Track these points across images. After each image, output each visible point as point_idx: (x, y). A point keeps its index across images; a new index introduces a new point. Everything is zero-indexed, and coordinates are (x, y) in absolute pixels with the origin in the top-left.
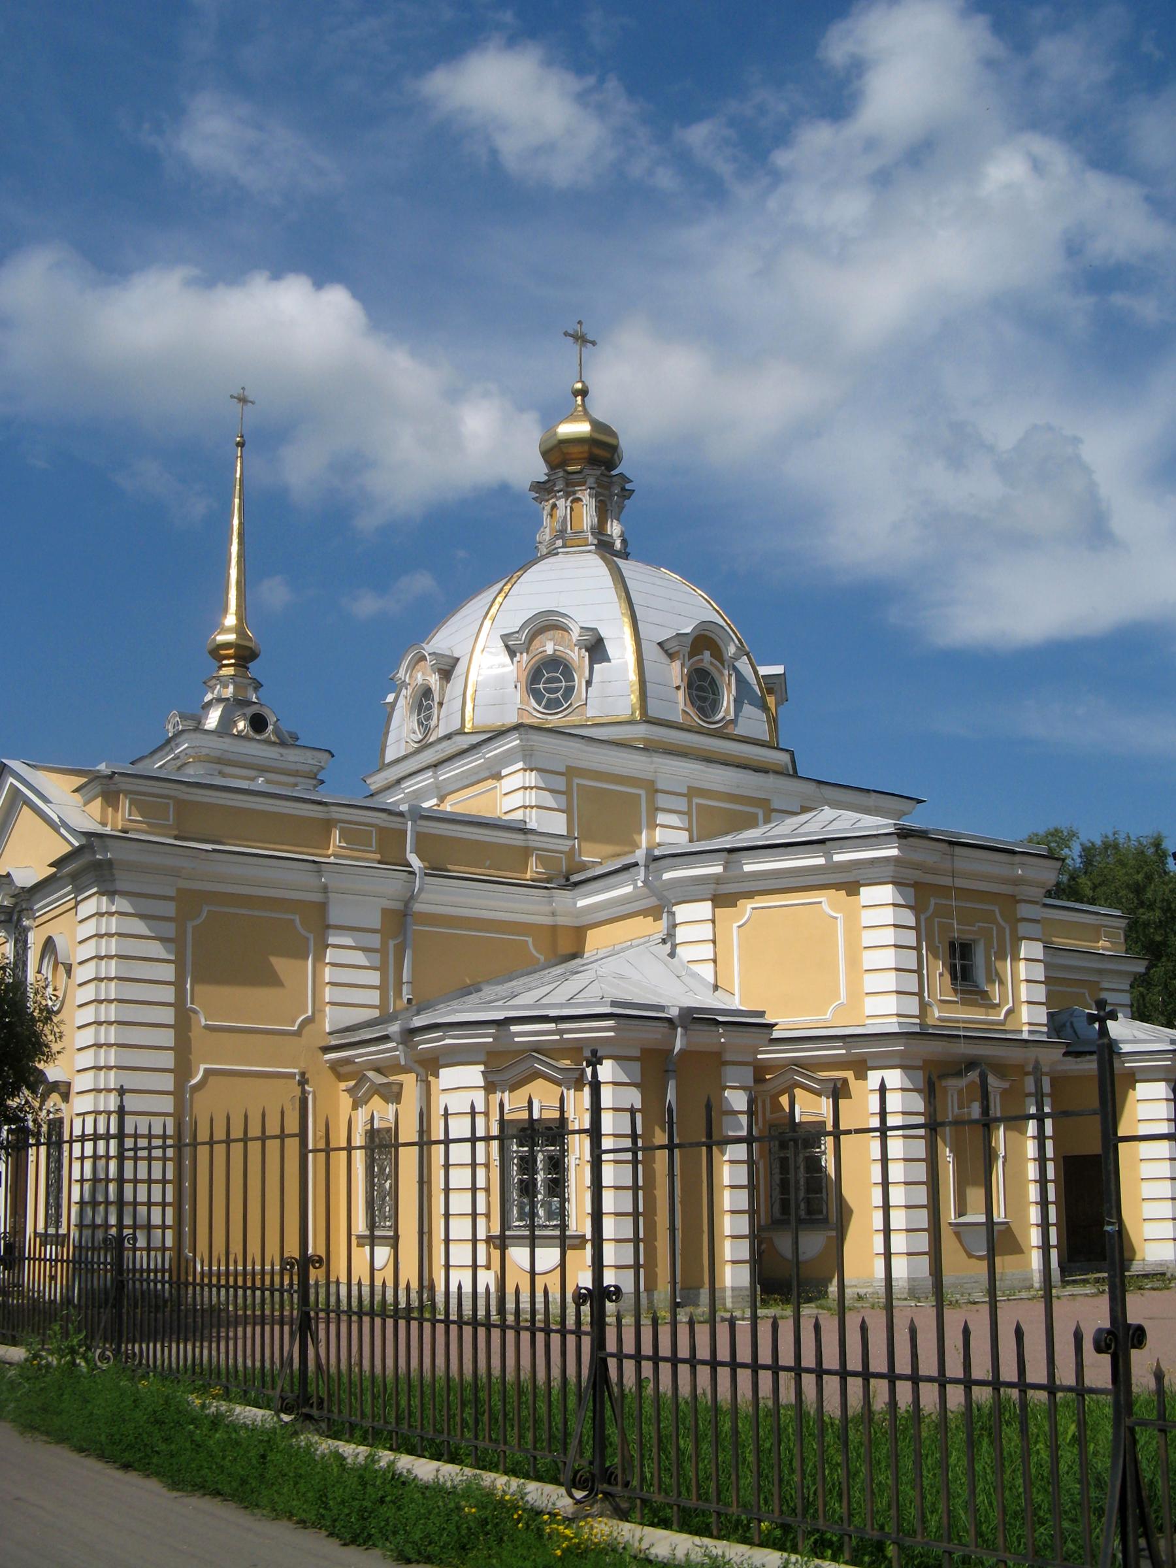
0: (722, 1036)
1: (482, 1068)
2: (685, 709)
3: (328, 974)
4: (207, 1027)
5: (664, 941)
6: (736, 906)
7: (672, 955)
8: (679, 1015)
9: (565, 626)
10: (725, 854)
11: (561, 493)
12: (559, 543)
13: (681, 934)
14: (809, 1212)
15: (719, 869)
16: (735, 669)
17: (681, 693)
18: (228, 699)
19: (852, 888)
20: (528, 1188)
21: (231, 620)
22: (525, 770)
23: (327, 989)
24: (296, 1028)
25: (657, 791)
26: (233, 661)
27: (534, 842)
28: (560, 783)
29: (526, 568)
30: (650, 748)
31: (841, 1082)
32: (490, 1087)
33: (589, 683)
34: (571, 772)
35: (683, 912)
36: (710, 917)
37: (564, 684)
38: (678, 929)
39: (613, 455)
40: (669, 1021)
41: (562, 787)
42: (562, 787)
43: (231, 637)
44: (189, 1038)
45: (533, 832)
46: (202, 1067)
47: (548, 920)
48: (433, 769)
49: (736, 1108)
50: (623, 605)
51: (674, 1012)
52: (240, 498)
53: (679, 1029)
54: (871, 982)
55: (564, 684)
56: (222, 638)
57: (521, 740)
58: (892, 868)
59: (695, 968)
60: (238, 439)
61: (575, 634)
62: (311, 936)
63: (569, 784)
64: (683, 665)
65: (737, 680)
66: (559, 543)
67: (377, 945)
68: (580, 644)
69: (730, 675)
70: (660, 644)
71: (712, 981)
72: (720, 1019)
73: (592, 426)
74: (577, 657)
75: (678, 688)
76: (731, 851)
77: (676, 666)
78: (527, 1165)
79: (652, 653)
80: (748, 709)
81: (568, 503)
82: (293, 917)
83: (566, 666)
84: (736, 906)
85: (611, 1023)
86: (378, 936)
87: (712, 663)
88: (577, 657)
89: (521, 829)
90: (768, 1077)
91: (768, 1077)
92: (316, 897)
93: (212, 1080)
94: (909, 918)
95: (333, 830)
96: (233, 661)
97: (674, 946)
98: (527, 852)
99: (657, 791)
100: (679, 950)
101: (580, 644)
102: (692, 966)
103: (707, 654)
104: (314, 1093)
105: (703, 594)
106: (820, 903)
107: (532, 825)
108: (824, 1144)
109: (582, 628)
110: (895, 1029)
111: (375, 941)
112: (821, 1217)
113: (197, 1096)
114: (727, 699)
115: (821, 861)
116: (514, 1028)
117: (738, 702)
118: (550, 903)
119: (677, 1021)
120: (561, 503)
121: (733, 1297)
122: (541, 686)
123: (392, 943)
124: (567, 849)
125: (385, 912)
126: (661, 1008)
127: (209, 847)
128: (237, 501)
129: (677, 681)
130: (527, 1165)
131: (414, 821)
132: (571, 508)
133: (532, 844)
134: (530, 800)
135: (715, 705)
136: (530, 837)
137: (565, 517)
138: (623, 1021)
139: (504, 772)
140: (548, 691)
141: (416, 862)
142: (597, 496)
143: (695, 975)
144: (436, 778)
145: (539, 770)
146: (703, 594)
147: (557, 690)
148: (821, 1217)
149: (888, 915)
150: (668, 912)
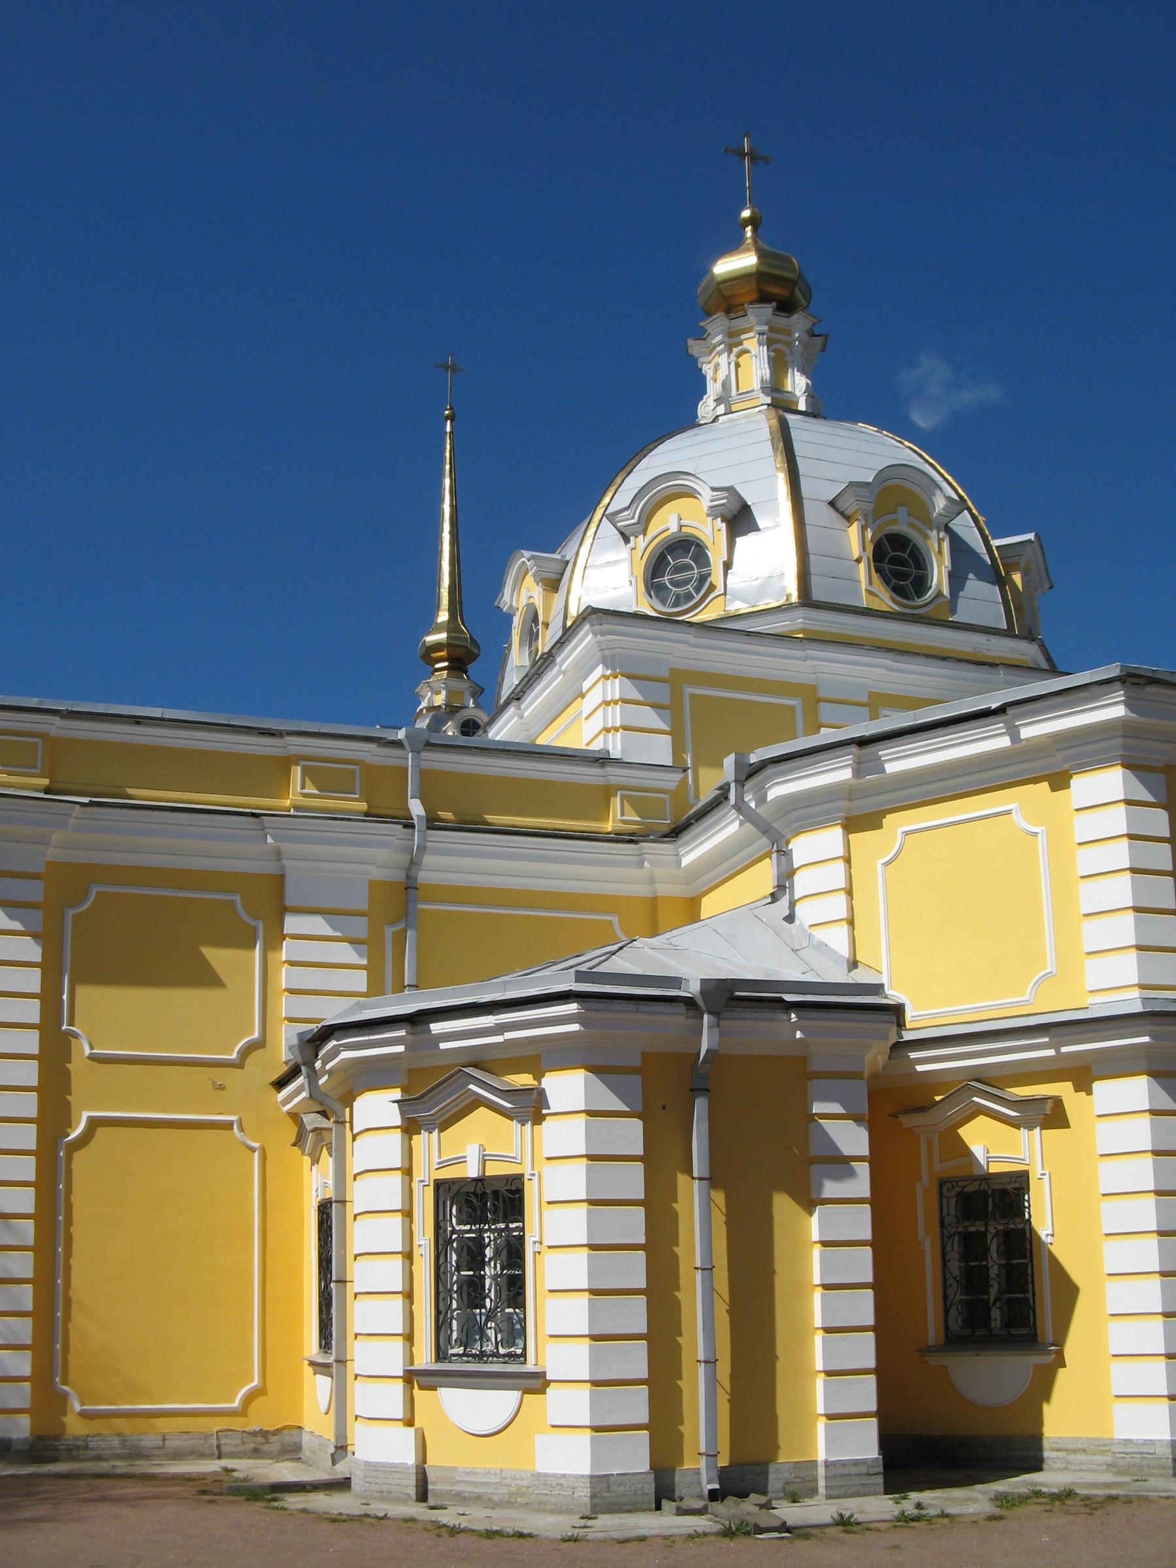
0: (796, 1027)
1: (397, 1094)
2: (870, 588)
3: (284, 977)
4: (92, 1057)
5: (774, 898)
6: (881, 827)
7: (790, 918)
8: (702, 992)
9: (684, 490)
10: (854, 749)
11: (722, 346)
12: (721, 409)
13: (802, 884)
14: (1008, 1323)
15: (846, 774)
16: (948, 529)
17: (862, 567)
18: (439, 707)
19: (1059, 782)
20: (473, 1292)
21: (443, 616)
22: (606, 678)
23: (284, 999)
24: (234, 1056)
25: (819, 700)
26: (446, 664)
27: (615, 775)
28: (663, 694)
29: (662, 440)
30: (814, 639)
31: (1050, 1104)
32: (410, 1128)
33: (728, 566)
34: (678, 678)
35: (804, 847)
36: (840, 852)
37: (696, 571)
38: (797, 878)
39: (793, 290)
40: (689, 1002)
41: (665, 700)
42: (665, 700)
43: (442, 636)
44: (68, 1072)
45: (618, 762)
46: (85, 1115)
47: (643, 890)
48: (515, 703)
49: (847, 1151)
50: (779, 458)
51: (693, 989)
52: (451, 479)
53: (706, 1016)
54: (1094, 934)
55: (696, 571)
56: (431, 639)
57: (595, 634)
58: (1120, 741)
59: (820, 934)
60: (447, 412)
61: (706, 498)
62: (260, 925)
63: (677, 694)
64: (863, 529)
65: (953, 549)
66: (721, 409)
67: (363, 935)
68: (714, 512)
69: (940, 541)
70: (832, 504)
71: (844, 951)
72: (789, 998)
73: (759, 258)
74: (712, 533)
75: (858, 561)
76: (863, 742)
77: (854, 530)
78: (473, 1255)
79: (817, 514)
80: (974, 586)
81: (733, 357)
82: (231, 898)
83: (698, 545)
84: (881, 827)
85: (572, 1008)
86: (364, 921)
87: (910, 525)
88: (712, 533)
89: (602, 760)
90: (938, 1098)
91: (938, 1098)
92: (269, 868)
93: (100, 1131)
94: (1158, 821)
95: (293, 768)
96: (446, 664)
97: (792, 904)
98: (607, 792)
99: (819, 700)
100: (799, 909)
101: (714, 512)
102: (814, 931)
103: (902, 512)
104: (263, 1151)
105: (911, 446)
106: (1008, 812)
107: (616, 753)
108: (1029, 1208)
109: (714, 489)
110: (1137, 1008)
111: (360, 927)
112: (1025, 1331)
113: (77, 1156)
114: (939, 574)
115: (1005, 742)
116: (436, 1028)
117: (957, 579)
118: (641, 865)
119: (700, 1002)
120: (723, 359)
121: (827, 1478)
122: (666, 578)
123: (389, 931)
124: (672, 786)
125: (373, 884)
126: (676, 982)
127: (86, 800)
128: (447, 482)
129: (856, 552)
130: (473, 1255)
131: (416, 751)
132: (737, 365)
133: (614, 780)
134: (614, 720)
135: (920, 585)
136: (610, 770)
137: (728, 376)
138: (593, 1004)
139: (585, 688)
140: (676, 584)
141: (416, 808)
142: (770, 343)
143: (822, 946)
144: (521, 717)
145: (629, 677)
146: (911, 446)
147: (686, 582)
148: (1025, 1331)
149: (1117, 820)
150: (778, 851)
